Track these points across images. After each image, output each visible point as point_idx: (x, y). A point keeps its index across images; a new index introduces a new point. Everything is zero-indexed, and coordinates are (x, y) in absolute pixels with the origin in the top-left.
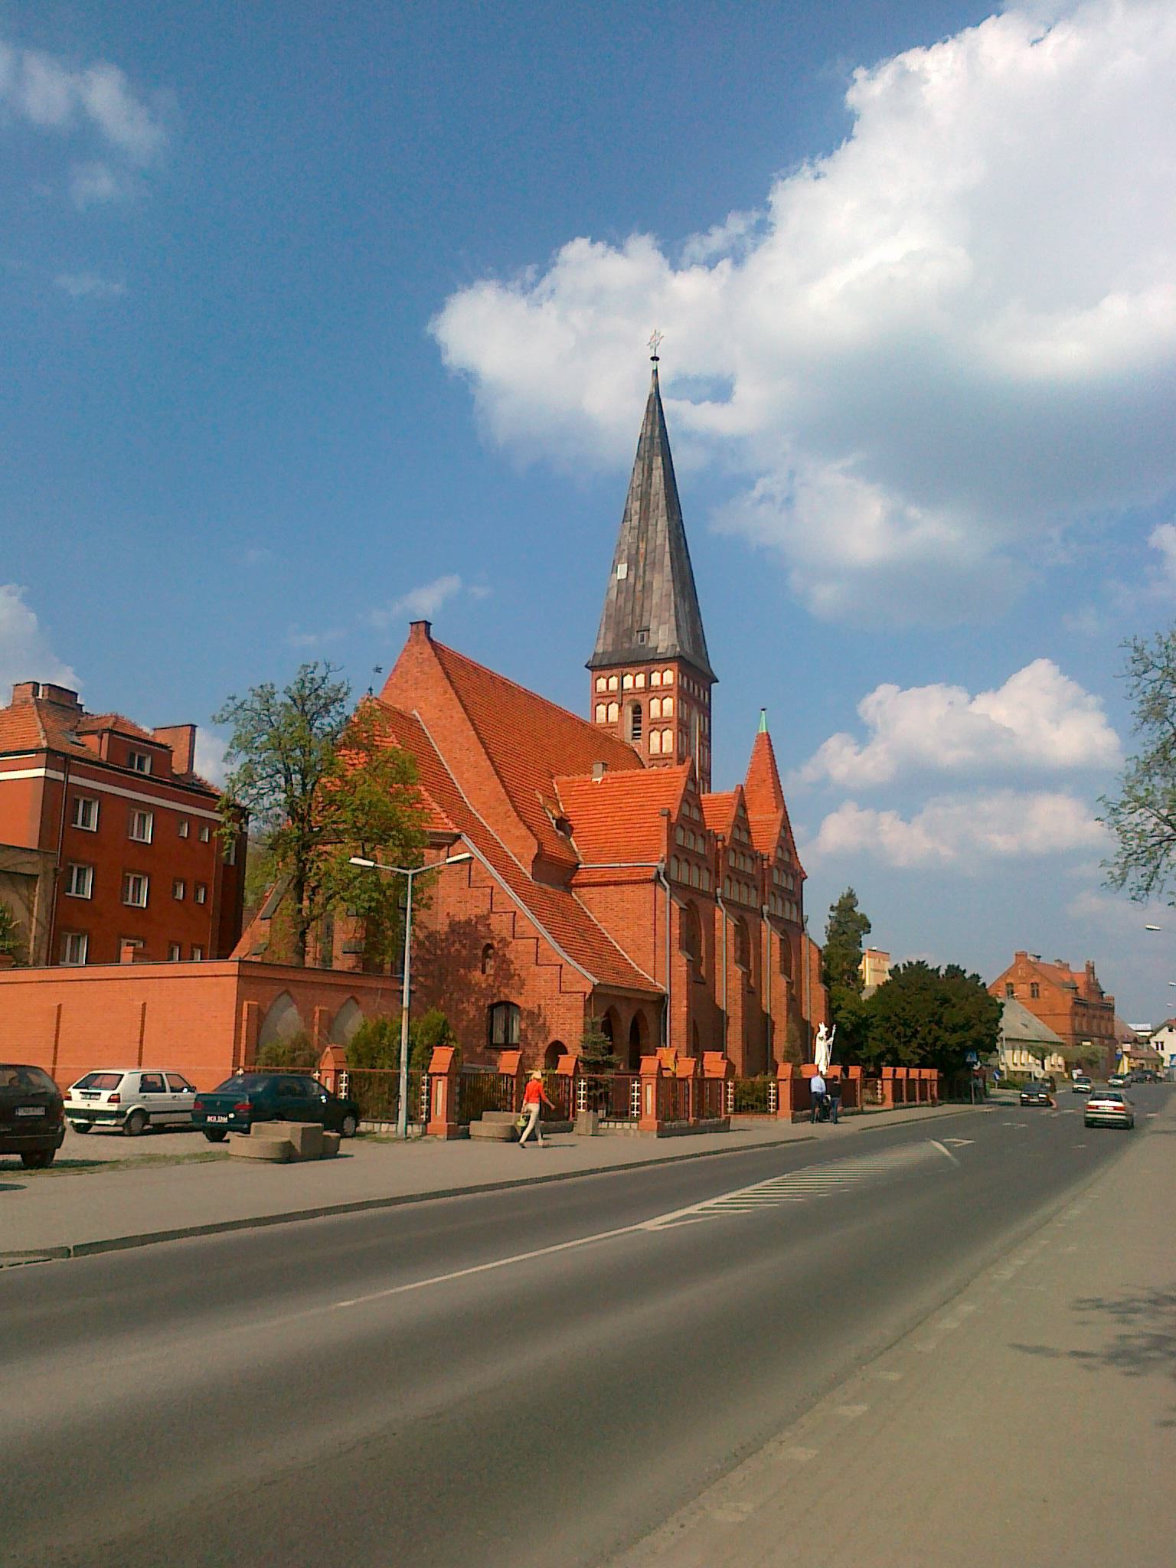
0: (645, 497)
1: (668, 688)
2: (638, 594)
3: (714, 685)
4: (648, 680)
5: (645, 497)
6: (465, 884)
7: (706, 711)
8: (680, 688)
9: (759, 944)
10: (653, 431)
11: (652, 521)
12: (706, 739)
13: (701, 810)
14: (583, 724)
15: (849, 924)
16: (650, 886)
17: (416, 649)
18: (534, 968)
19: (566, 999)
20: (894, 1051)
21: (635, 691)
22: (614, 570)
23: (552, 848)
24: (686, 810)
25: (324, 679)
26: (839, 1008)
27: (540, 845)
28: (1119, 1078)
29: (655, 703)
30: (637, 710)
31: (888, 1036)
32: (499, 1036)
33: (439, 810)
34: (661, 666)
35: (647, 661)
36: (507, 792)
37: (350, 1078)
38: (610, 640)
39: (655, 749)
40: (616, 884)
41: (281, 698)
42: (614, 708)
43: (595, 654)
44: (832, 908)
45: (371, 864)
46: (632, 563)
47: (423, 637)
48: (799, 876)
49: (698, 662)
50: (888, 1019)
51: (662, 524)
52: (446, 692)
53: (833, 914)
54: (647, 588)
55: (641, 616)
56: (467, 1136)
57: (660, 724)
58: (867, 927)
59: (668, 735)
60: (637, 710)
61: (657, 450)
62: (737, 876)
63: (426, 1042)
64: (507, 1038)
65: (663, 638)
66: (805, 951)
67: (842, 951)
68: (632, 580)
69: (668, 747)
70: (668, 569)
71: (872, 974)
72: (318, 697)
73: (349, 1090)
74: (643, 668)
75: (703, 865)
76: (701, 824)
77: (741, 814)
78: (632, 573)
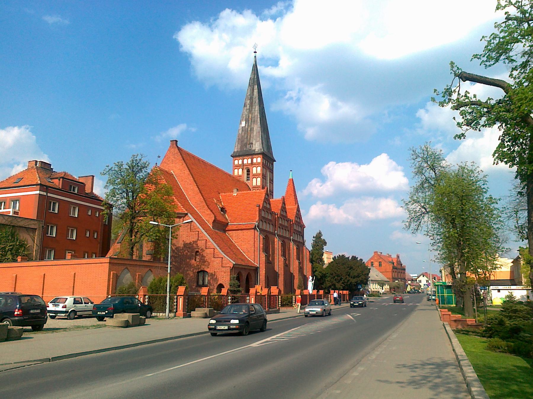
0: (251, 99)
1: (259, 164)
4: (252, 161)
5: (251, 99)
6: (189, 230)
7: (272, 171)
8: (263, 164)
9: (289, 250)
10: (254, 76)
11: (254, 107)
12: (272, 181)
13: (270, 204)
14: (230, 175)
15: (320, 242)
16: (253, 230)
17: (173, 150)
18: (213, 259)
19: (224, 269)
20: (334, 285)
21: (248, 164)
22: (241, 123)
23: (220, 218)
25: (140, 160)
26: (316, 271)
27: (215, 217)
30: (248, 171)
31: (332, 280)
32: (201, 282)
33: (180, 205)
34: (257, 156)
35: (251, 154)
36: (204, 199)
37: (149, 298)
38: (239, 147)
39: (254, 184)
40: (241, 230)
41: (125, 166)
42: (240, 170)
44: (314, 237)
45: (157, 223)
46: (247, 121)
47: (175, 146)
48: (303, 227)
49: (269, 155)
50: (332, 274)
53: (314, 239)
54: (252, 130)
56: (190, 316)
57: (256, 176)
58: (325, 243)
59: (259, 179)
60: (248, 171)
61: (255, 83)
62: (282, 227)
63: (176, 284)
64: (203, 283)
65: (257, 146)
66: (304, 251)
67: (317, 252)
68: (247, 127)
69: (259, 183)
70: (259, 123)
71: (327, 259)
72: (138, 166)
73: (149, 302)
74: (250, 157)
75: (271, 223)
76: (270, 209)
78: (247, 125)
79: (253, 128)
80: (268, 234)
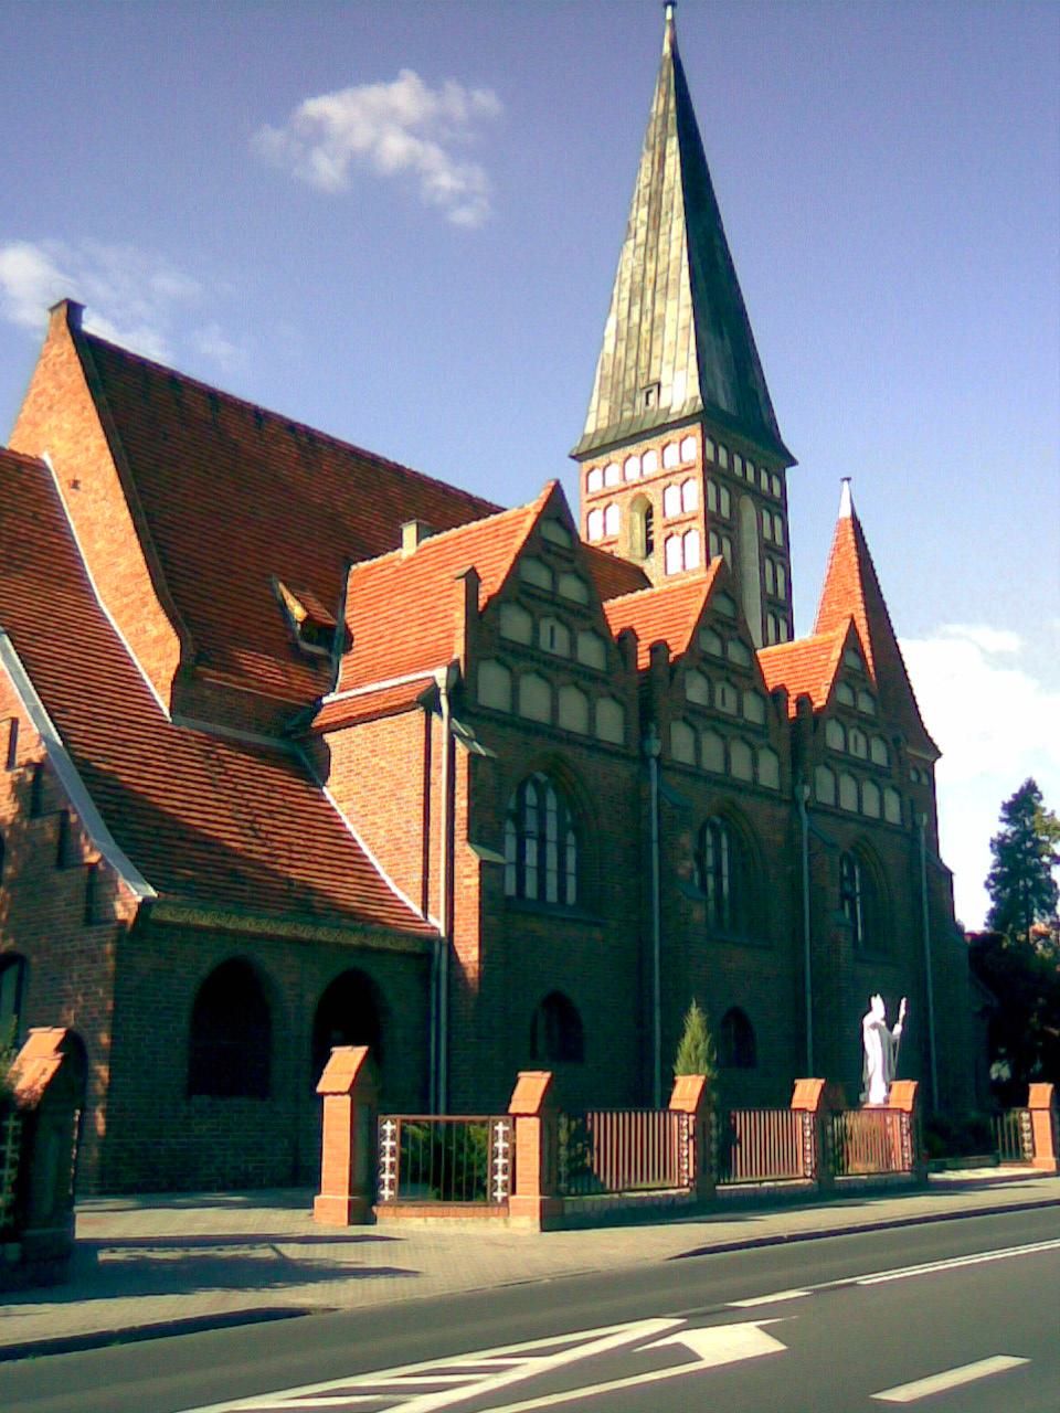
2: (645, 335)
3: (790, 472)
11: (664, 229)
16: (416, 717)
24: (844, 696)
28: (692, 877)
29: (673, 494)
43: (584, 437)
51: (676, 226)
52: (84, 408)
54: (656, 325)
55: (649, 366)
65: (681, 388)
77: (724, 606)
79: (663, 317)
80: (568, 752)
